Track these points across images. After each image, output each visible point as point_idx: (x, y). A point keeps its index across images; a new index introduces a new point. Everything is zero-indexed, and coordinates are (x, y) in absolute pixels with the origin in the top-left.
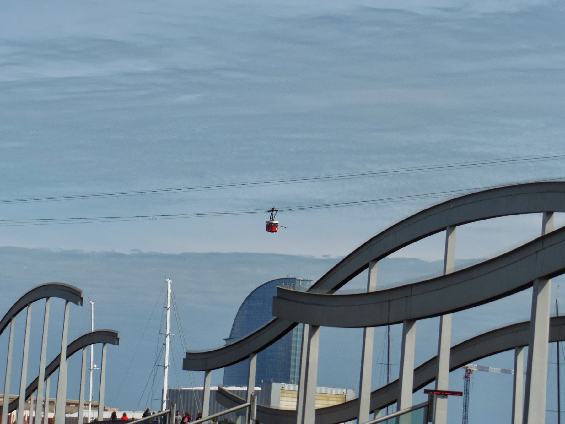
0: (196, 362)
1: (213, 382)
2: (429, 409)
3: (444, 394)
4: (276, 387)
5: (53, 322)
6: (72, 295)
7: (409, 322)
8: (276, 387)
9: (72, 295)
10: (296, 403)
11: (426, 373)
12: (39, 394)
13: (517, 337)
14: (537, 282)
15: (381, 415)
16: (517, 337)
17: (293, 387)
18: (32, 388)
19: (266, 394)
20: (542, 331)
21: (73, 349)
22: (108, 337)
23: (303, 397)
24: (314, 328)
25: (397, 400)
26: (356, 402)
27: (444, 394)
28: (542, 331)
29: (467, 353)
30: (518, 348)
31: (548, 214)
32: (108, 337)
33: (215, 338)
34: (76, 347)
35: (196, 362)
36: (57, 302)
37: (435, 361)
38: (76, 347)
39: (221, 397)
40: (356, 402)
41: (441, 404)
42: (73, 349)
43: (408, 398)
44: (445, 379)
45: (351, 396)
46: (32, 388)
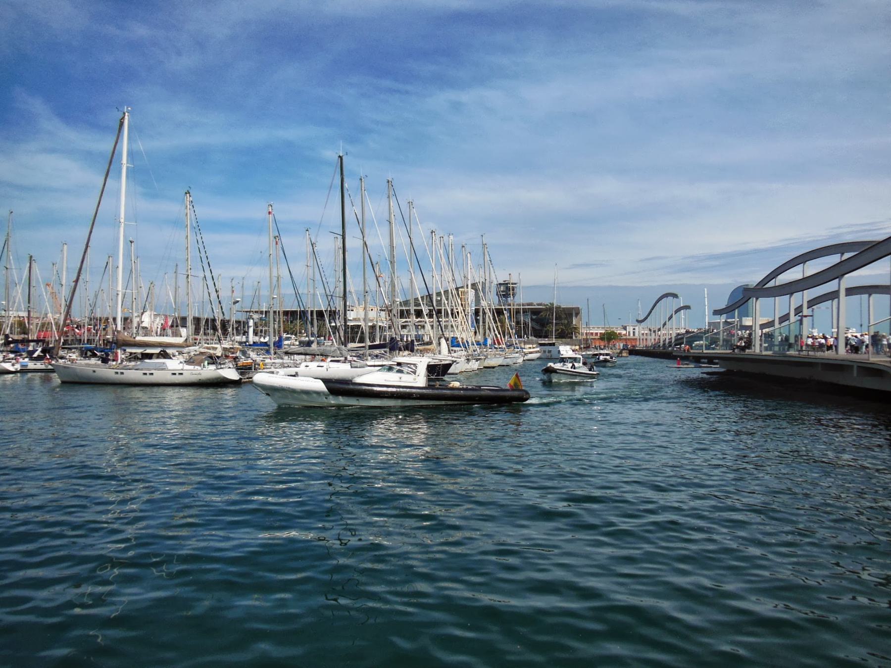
0: (717, 312)
1: (722, 319)
2: (801, 322)
3: (806, 316)
4: (744, 319)
5: (669, 305)
6: (675, 296)
7: (792, 294)
8: (744, 319)
9: (675, 296)
10: (875, 297)
11: (799, 310)
12: (666, 326)
13: (833, 295)
14: (840, 276)
15: (783, 324)
16: (833, 295)
17: (350, 324)
18: (665, 324)
19: (741, 321)
20: (842, 293)
21: (676, 312)
22: (687, 307)
23: (755, 320)
24: (757, 299)
25: (788, 319)
26: (773, 321)
27: (806, 316)
28: (842, 293)
29: (812, 303)
30: (833, 299)
31: (842, 254)
32: (687, 307)
33: (723, 305)
34: (677, 311)
35: (717, 312)
36: (670, 298)
37: (801, 306)
38: (677, 311)
39: (726, 323)
40: (773, 321)
41: (804, 319)
42: (676, 312)
43: (793, 318)
44: (806, 311)
45: (771, 320)
46: (665, 324)
